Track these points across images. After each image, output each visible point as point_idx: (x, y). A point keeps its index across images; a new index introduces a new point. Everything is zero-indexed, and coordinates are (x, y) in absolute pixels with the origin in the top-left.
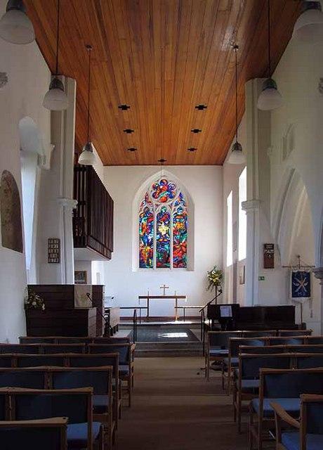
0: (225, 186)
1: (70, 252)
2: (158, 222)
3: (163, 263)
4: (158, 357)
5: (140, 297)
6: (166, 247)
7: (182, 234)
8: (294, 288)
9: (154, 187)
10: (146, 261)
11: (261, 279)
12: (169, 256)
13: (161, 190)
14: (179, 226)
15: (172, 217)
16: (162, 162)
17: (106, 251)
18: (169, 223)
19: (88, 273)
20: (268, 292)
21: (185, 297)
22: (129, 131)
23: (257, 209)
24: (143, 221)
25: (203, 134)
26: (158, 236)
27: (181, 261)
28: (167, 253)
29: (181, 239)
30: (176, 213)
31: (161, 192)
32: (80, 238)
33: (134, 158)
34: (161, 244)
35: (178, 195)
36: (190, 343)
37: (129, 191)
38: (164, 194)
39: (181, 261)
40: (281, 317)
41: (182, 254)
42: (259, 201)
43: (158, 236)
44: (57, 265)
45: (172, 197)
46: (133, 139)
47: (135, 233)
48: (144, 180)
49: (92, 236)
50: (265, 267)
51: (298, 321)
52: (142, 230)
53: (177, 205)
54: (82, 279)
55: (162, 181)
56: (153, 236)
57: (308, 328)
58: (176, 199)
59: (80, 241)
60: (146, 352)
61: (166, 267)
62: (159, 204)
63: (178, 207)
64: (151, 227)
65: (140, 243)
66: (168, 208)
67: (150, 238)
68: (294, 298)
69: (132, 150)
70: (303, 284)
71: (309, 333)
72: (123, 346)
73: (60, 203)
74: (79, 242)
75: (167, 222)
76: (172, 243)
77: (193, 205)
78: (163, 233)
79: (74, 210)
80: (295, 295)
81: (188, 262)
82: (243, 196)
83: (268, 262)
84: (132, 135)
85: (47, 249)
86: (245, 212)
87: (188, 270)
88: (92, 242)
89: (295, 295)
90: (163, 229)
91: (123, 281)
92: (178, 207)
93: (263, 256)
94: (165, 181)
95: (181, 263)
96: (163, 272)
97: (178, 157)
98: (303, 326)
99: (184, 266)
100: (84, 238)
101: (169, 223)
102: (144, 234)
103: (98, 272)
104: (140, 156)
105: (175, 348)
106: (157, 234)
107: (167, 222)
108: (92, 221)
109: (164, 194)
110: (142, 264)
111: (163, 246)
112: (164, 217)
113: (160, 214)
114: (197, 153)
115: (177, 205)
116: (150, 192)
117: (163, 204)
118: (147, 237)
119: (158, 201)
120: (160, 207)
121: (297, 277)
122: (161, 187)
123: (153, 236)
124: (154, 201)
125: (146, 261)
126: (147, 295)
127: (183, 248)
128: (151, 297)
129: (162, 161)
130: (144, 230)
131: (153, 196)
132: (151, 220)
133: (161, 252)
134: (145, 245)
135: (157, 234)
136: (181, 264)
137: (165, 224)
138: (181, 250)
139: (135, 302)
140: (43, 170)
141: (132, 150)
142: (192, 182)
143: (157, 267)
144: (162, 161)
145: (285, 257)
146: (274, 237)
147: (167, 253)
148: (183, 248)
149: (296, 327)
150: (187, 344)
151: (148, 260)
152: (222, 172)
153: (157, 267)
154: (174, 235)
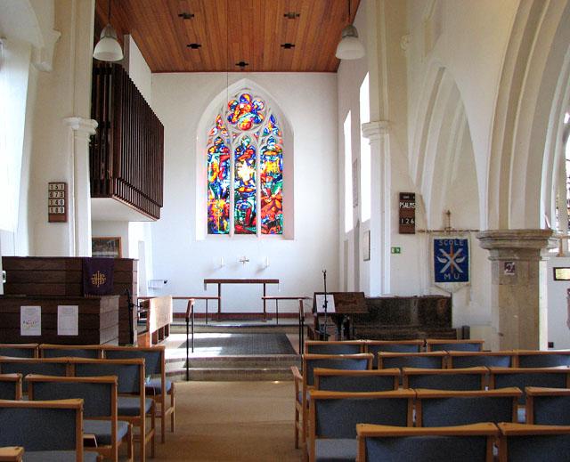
0: (340, 104)
1: (84, 206)
2: (237, 160)
3: (247, 225)
4: (239, 380)
5: (207, 281)
6: (250, 200)
7: (275, 181)
8: (438, 266)
9: (231, 106)
10: (218, 224)
11: (396, 252)
12: (254, 215)
13: (241, 111)
14: (272, 167)
15: (260, 152)
16: (242, 66)
17: (150, 202)
18: (255, 161)
19: (123, 242)
20: (391, 272)
21: (276, 281)
22: (186, 16)
23: (387, 136)
24: (213, 160)
25: (302, 22)
26: (238, 183)
27: (273, 224)
28: (253, 213)
29: (273, 188)
30: (265, 147)
31: (241, 113)
32: (102, 182)
33: (197, 59)
34: (241, 196)
35: (268, 118)
36: (281, 359)
37: (193, 112)
38: (246, 118)
39: (273, 224)
40: (434, 313)
41: (276, 212)
42: (390, 119)
43: (238, 183)
44: (64, 224)
45: (258, 122)
46: (195, 30)
47: (201, 178)
48: (213, 96)
49: (121, 180)
50: (402, 232)
51: (457, 322)
52: (213, 171)
53: (266, 133)
54: (113, 250)
55: (242, 97)
56: (229, 183)
57: (473, 338)
58: (266, 125)
59: (101, 186)
60: (208, 372)
61: (250, 233)
62: (237, 132)
63: (268, 138)
64: (226, 169)
65: (209, 193)
66: (253, 139)
67: (224, 186)
68: (437, 283)
69: (195, 46)
70: (451, 261)
71: (478, 345)
72: (128, 365)
73: (69, 124)
74: (100, 188)
75: (251, 162)
76: (259, 194)
77: (292, 136)
78: (246, 179)
79: (92, 137)
80: (439, 278)
81: (284, 225)
82: (365, 116)
83: (406, 223)
84: (192, 21)
85: (46, 203)
86: (368, 140)
87: (286, 238)
88: (123, 188)
89: (439, 278)
90: (245, 172)
91: (174, 253)
92: (268, 138)
93: (397, 213)
94: (246, 97)
95: (273, 227)
96: (245, 239)
97: (266, 59)
98: (465, 332)
99: (279, 231)
100: (108, 181)
101: (255, 161)
102: (216, 179)
103: (141, 239)
104: (207, 58)
105: (248, 366)
106: (236, 180)
107: (251, 162)
108: (125, 150)
109: (246, 118)
110: (212, 228)
111: (245, 198)
112: (247, 154)
113: (241, 148)
114: (296, 51)
115: (266, 133)
116: (224, 113)
117: (244, 133)
118: (220, 185)
119: (236, 128)
120: (241, 137)
121: (443, 247)
122: (242, 106)
123: (229, 183)
124: (231, 127)
125: (218, 224)
126: (323, 291)
127: (277, 203)
128: (323, 293)
129: (242, 64)
130: (215, 174)
131: (230, 120)
132: (225, 158)
133: (242, 209)
134: (216, 198)
135: (236, 180)
136: (274, 228)
137: (249, 164)
138: (274, 205)
139: (198, 289)
140: (42, 71)
141: (195, 46)
142: (291, 99)
143: (236, 233)
144: (242, 64)
145: (430, 218)
146: (415, 182)
147: (253, 213)
148: (277, 203)
149: (453, 334)
150: (275, 359)
151: (221, 222)
152: (337, 80)
153: (236, 233)
154: (263, 182)
